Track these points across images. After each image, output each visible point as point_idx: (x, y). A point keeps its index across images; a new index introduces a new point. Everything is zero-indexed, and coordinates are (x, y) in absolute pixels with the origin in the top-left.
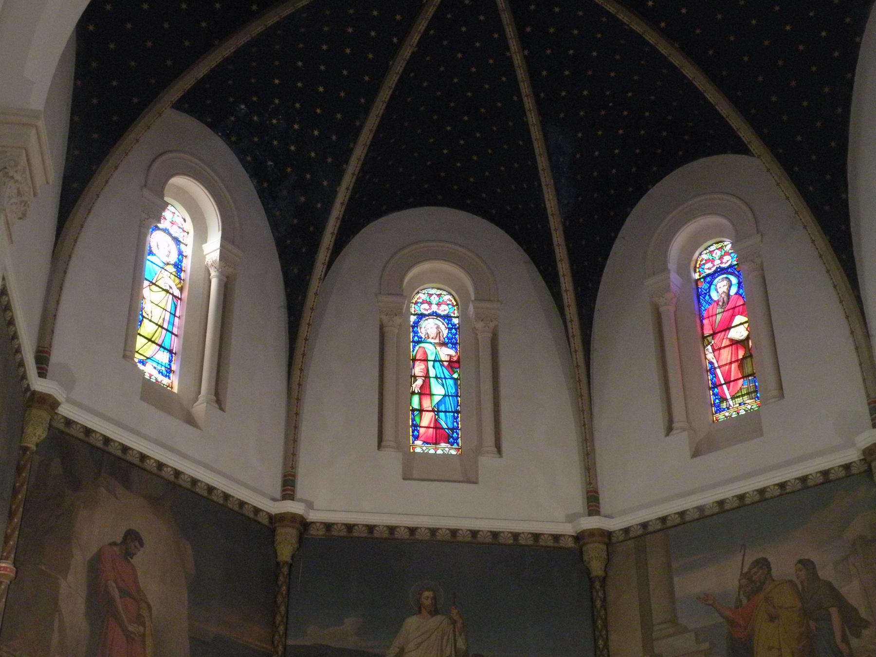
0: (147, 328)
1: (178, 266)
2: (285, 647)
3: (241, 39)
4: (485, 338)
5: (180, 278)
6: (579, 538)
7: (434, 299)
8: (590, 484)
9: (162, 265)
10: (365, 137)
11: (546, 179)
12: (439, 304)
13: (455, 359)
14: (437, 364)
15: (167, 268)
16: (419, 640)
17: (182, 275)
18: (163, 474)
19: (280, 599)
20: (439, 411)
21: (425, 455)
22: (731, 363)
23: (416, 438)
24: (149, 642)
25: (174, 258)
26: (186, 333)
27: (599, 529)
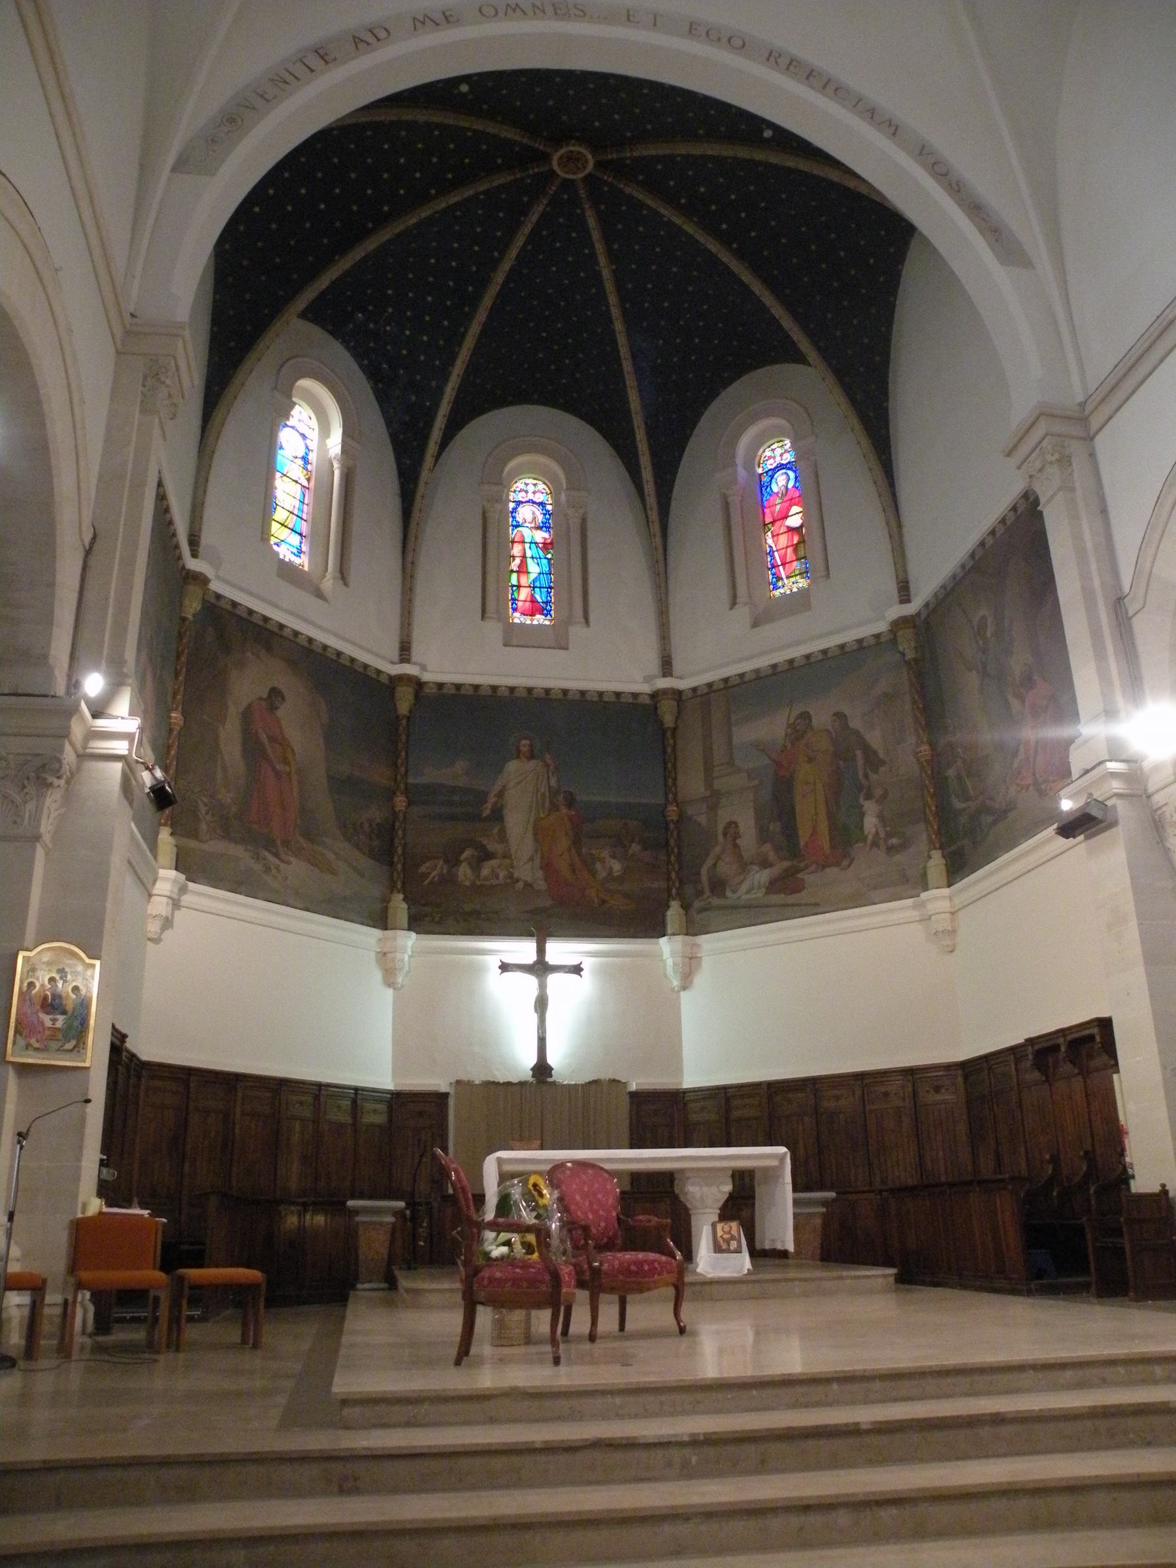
0: (279, 515)
1: (305, 459)
2: (406, 784)
3: (357, 254)
4: (575, 523)
5: (307, 470)
6: (654, 696)
7: (531, 488)
8: (665, 650)
9: (292, 459)
10: (469, 343)
11: (631, 381)
12: (534, 493)
13: (549, 541)
14: (533, 545)
15: (295, 460)
16: (520, 779)
17: (309, 467)
18: (298, 640)
19: (400, 746)
20: (534, 587)
21: (522, 625)
22: (787, 547)
23: (515, 610)
24: (295, 777)
25: (301, 453)
26: (313, 519)
27: (672, 689)
